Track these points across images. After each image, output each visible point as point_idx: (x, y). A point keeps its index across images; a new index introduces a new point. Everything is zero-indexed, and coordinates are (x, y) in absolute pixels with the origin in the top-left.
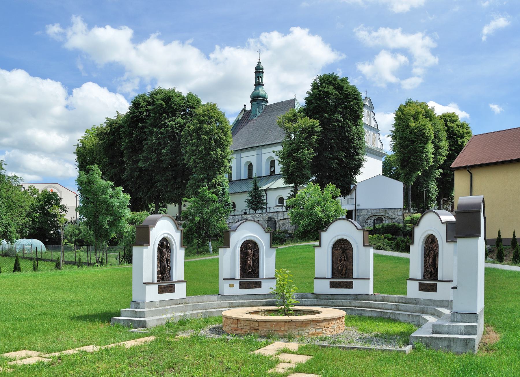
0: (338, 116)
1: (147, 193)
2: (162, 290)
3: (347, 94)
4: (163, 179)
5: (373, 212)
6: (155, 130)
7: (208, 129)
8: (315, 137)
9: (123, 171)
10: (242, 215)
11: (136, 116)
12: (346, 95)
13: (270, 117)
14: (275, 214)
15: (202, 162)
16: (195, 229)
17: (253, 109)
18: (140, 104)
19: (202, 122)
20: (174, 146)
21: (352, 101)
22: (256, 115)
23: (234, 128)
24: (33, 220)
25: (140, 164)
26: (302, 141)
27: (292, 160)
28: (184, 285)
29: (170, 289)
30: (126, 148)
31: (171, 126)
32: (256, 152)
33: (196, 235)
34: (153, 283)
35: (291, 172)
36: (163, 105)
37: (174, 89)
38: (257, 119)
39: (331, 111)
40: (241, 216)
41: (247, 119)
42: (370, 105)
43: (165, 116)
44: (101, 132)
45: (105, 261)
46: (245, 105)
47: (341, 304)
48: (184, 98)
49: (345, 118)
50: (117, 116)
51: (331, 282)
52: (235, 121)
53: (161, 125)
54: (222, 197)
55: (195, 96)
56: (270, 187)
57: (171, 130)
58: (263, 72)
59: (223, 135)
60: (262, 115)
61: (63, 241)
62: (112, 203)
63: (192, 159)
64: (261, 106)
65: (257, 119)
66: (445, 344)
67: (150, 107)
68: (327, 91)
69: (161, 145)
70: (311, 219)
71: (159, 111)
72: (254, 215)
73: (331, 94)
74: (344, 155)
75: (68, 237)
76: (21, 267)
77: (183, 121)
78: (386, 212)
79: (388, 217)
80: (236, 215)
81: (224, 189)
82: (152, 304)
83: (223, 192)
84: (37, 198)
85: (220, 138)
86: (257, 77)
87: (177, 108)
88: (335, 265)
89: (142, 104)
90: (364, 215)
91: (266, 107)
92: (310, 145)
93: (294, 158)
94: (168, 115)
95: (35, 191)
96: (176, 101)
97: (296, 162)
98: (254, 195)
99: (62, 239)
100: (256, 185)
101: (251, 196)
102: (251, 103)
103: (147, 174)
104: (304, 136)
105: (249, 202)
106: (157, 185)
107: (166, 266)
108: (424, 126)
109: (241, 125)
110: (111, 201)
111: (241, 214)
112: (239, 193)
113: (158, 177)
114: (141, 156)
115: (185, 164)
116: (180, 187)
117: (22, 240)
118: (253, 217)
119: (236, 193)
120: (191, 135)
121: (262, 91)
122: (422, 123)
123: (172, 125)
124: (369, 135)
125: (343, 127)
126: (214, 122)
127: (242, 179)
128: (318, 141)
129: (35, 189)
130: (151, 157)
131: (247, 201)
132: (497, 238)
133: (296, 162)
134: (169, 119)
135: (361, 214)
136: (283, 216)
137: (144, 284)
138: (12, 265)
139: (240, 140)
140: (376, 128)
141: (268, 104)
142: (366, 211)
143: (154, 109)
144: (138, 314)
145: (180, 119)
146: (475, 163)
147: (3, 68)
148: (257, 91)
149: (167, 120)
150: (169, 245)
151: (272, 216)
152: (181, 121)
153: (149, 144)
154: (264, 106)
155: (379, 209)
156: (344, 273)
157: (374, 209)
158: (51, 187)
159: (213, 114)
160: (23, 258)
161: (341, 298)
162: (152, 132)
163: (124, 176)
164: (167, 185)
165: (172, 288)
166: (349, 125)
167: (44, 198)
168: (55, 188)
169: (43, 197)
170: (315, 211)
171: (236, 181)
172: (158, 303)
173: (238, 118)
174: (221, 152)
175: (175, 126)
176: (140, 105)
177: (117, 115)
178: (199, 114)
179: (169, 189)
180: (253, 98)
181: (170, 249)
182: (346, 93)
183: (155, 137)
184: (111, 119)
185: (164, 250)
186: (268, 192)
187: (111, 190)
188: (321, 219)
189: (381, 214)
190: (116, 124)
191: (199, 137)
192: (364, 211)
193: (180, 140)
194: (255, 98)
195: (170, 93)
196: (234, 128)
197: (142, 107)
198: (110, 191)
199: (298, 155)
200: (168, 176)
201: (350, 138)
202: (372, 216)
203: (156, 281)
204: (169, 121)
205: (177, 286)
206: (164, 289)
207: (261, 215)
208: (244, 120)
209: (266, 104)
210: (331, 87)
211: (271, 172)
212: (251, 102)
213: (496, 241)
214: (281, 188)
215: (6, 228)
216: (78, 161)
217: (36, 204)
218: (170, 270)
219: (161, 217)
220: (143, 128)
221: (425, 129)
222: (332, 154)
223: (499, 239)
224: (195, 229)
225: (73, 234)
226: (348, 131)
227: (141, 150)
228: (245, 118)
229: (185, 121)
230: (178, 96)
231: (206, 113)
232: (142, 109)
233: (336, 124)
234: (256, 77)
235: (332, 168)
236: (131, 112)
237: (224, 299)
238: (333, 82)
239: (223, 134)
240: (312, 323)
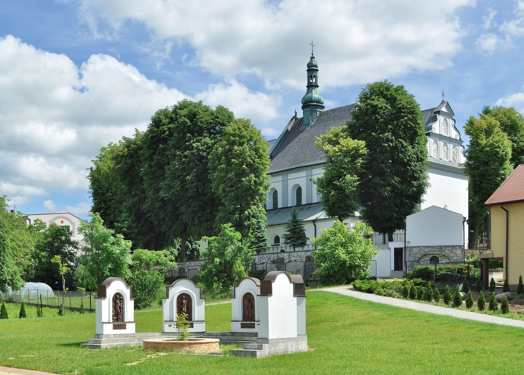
0: (388, 135)
1: (172, 226)
2: (115, 327)
3: (400, 107)
4: (189, 210)
5: (426, 250)
6: (178, 153)
7: (238, 152)
9: (142, 201)
10: (277, 253)
11: (156, 136)
13: (324, 128)
15: (233, 191)
16: (215, 272)
17: (305, 117)
18: (161, 121)
19: (233, 143)
20: (201, 171)
21: (405, 116)
22: (309, 124)
23: (281, 142)
24: (40, 262)
25: (162, 194)
26: (344, 166)
27: (332, 189)
28: (134, 324)
29: (123, 327)
30: (146, 174)
31: (197, 148)
33: (216, 278)
34: (109, 323)
35: (333, 203)
36: (187, 123)
37: (201, 102)
38: (310, 130)
39: (380, 128)
40: (276, 255)
41: (297, 130)
42: (448, 111)
43: (190, 137)
44: (117, 155)
45: (481, 312)
47: (246, 339)
48: (212, 114)
49: (397, 136)
50: (136, 135)
51: (241, 324)
52: (283, 133)
53: (185, 147)
54: (257, 232)
55: (226, 110)
56: (319, 217)
57: (196, 152)
58: (318, 70)
59: (258, 158)
60: (315, 125)
61: (64, 289)
62: (112, 251)
63: (221, 188)
65: (310, 130)
66: (244, 354)
67: (172, 126)
68: (375, 105)
70: (334, 261)
71: (182, 130)
72: (291, 253)
74: (399, 180)
75: (79, 279)
76: (27, 313)
77: (211, 142)
78: (442, 249)
79: (444, 256)
80: (270, 254)
81: (259, 222)
82: (108, 336)
83: (257, 225)
84: (44, 233)
85: (254, 162)
86: (310, 77)
87: (204, 125)
88: (245, 311)
89: (163, 121)
90: (416, 254)
91: (322, 114)
92: (353, 171)
93: (335, 187)
94: (193, 135)
95: (42, 225)
96: (202, 118)
97: (336, 192)
98: (292, 230)
99: (64, 287)
100: (294, 216)
101: (289, 231)
102: (302, 109)
103: (171, 204)
104: (346, 160)
105: (287, 238)
106: (182, 218)
107: (119, 312)
108: (497, 142)
109: (289, 138)
110: (111, 249)
111: (276, 252)
112: (283, 224)
113: (183, 209)
114: (162, 185)
115: (214, 194)
116: (209, 220)
117: (28, 284)
118: (289, 256)
119: (279, 224)
120: (219, 159)
122: (497, 139)
123: (198, 146)
124: (447, 149)
125: (395, 148)
126: (246, 143)
127: (289, 206)
128: (364, 166)
129: (41, 223)
130: (175, 185)
131: (283, 236)
132: (518, 284)
133: (336, 192)
134: (195, 140)
135: (412, 252)
137: (103, 323)
138: (18, 312)
139: (288, 157)
140: (458, 138)
141: (325, 110)
142: (418, 249)
143: (177, 127)
144: (98, 342)
145: (207, 140)
146: (509, 199)
147: (1, 36)
148: (310, 95)
149: (192, 141)
150: (121, 297)
151: (310, 255)
152: (208, 142)
153: (171, 169)
154: (318, 113)
155: (434, 247)
156: (250, 317)
157: (427, 247)
158: (60, 218)
159: (245, 133)
160: (29, 304)
161: (248, 335)
162: (175, 156)
163: (144, 207)
164: (193, 218)
165: (124, 327)
166: (402, 145)
167: (52, 234)
168: (66, 218)
169: (51, 233)
170: (337, 253)
171: (282, 208)
172: (112, 336)
173: (286, 129)
174: (254, 179)
175: (201, 148)
176: (161, 122)
178: (230, 134)
179: (196, 222)
180: (305, 104)
181: (123, 300)
183: (178, 162)
184: (128, 138)
185: (118, 301)
186: (318, 224)
187: (112, 237)
188: (344, 262)
189: (436, 253)
190: (134, 144)
191: (229, 163)
192: (415, 249)
193: (207, 163)
194: (307, 104)
195: (195, 108)
196: (281, 142)
197: (164, 125)
198: (112, 239)
199: (339, 184)
200: (194, 207)
201: (406, 161)
202: (425, 255)
203: (111, 321)
204: (194, 142)
205: (128, 325)
206: (117, 327)
208: (294, 131)
209: (321, 111)
210: (381, 100)
212: (303, 108)
213: (517, 286)
215: (12, 276)
216: (91, 188)
217: (43, 241)
218: (123, 314)
219: (115, 279)
220: (164, 150)
221: (499, 147)
222: (384, 180)
224: (215, 272)
225: (84, 276)
226: (402, 152)
227: (162, 176)
228: (296, 128)
229: (213, 141)
230: (206, 111)
231: (237, 132)
232: (163, 127)
233: (386, 145)
234: (308, 77)
235: (384, 196)
236: (151, 131)
237: (165, 335)
238: (385, 92)
239: (257, 157)
240: (187, 344)
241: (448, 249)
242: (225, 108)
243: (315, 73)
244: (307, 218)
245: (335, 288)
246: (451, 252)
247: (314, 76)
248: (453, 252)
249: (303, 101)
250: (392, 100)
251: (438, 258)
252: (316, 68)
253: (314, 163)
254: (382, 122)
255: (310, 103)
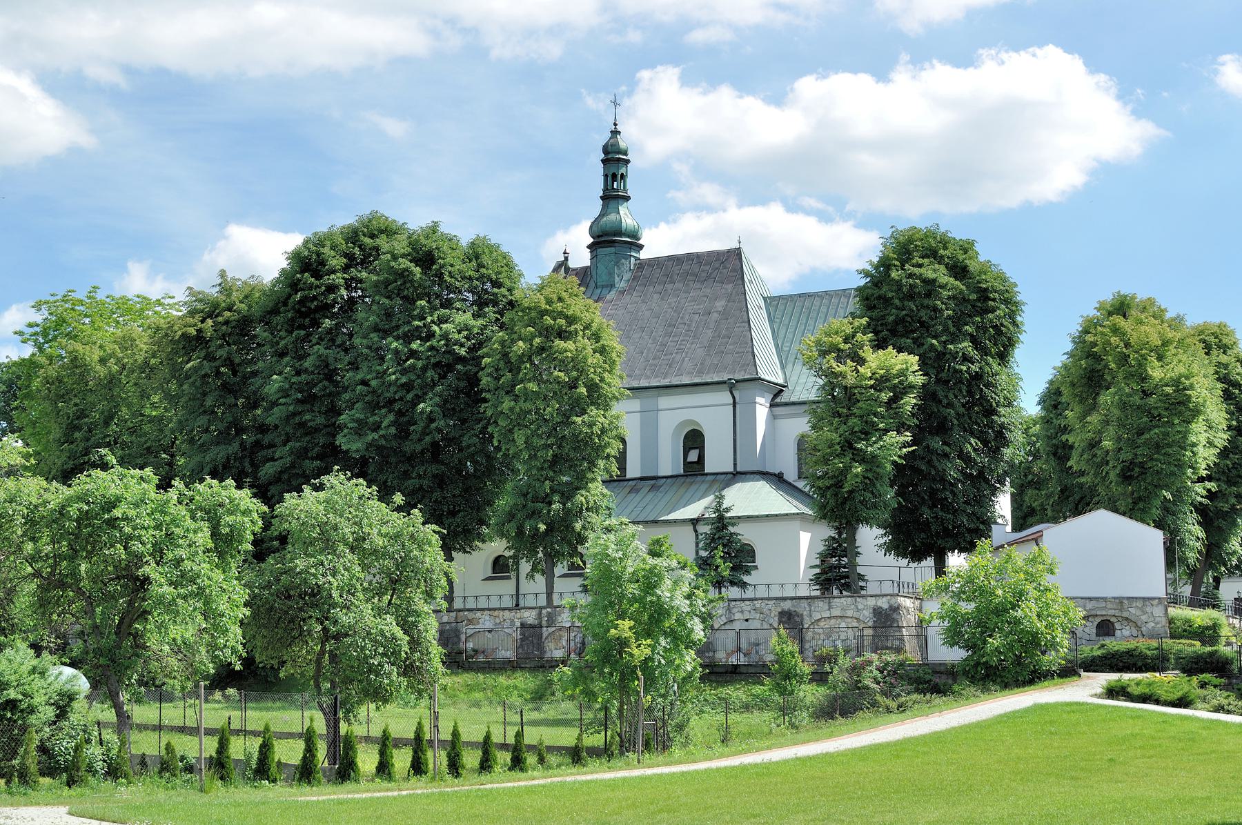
0: (966, 345)
8: (910, 401)
11: (315, 298)
12: (984, 294)
14: (804, 603)
22: (612, 286)
27: (853, 460)
31: (445, 336)
32: (639, 406)
46: (565, 253)
50: (220, 285)
58: (628, 161)
64: (626, 259)
69: (413, 389)
72: (733, 603)
73: (943, 287)
78: (1122, 605)
79: (1127, 619)
91: (642, 265)
108: (1187, 378)
118: (729, 609)
121: (626, 216)
125: (978, 377)
136: (829, 610)
148: (612, 217)
151: (792, 609)
155: (1105, 599)
157: (1090, 599)
177: (219, 281)
180: (599, 236)
182: (984, 286)
189: (1110, 612)
207: (758, 606)
211: (687, 464)
214: (748, 517)
223: (1001, 611)
234: (606, 176)
241: (1134, 605)
242: (493, 242)
243: (624, 168)
244: (669, 513)
245: (1043, 693)
246: (1143, 611)
247: (622, 175)
248: (1145, 613)
249: (595, 228)
250: (959, 271)
251: (1113, 624)
252: (624, 157)
253: (666, 382)
254: (949, 317)
255: (615, 235)
